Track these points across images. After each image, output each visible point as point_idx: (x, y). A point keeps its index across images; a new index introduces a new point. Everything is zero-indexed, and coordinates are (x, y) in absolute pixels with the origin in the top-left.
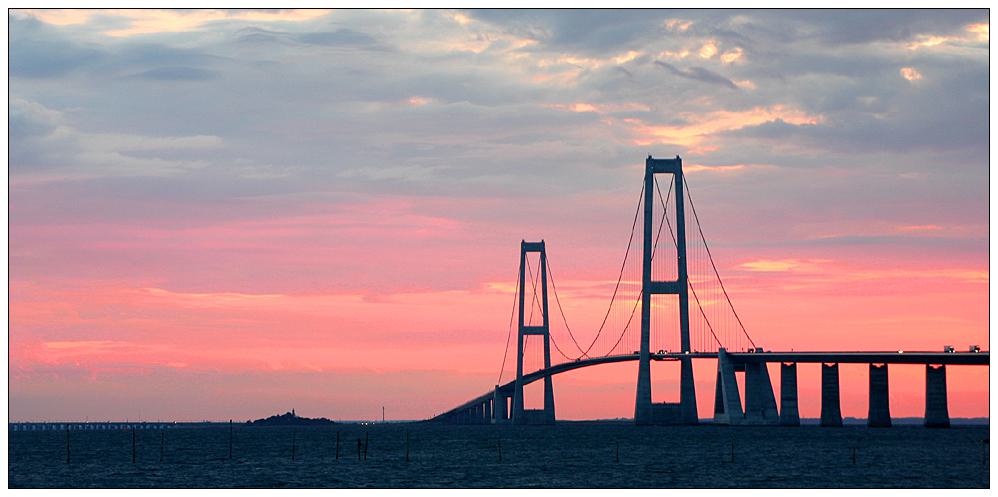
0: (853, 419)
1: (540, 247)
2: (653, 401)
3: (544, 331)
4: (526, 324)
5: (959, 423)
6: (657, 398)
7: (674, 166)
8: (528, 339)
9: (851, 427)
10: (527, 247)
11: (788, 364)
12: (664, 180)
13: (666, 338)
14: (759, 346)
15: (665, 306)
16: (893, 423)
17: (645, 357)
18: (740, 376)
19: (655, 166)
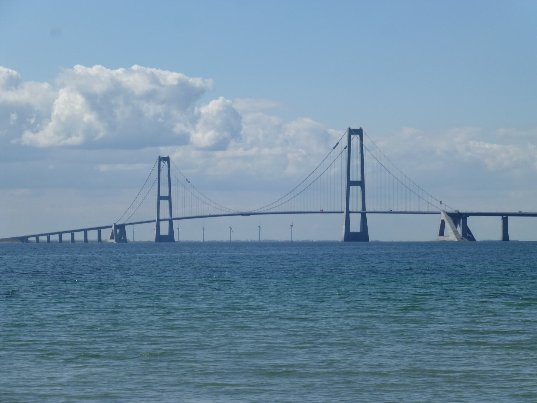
0: (515, 240)
1: (359, 132)
2: (160, 235)
3: (361, 183)
4: (351, 179)
5: (66, 241)
6: (352, 230)
7: (167, 159)
8: (161, 202)
9: (42, 242)
10: (351, 132)
11: (505, 217)
12: (164, 165)
13: (164, 214)
14: (391, 209)
15: (164, 204)
16: (39, 241)
17: (159, 220)
18: (118, 230)
19: (161, 159)
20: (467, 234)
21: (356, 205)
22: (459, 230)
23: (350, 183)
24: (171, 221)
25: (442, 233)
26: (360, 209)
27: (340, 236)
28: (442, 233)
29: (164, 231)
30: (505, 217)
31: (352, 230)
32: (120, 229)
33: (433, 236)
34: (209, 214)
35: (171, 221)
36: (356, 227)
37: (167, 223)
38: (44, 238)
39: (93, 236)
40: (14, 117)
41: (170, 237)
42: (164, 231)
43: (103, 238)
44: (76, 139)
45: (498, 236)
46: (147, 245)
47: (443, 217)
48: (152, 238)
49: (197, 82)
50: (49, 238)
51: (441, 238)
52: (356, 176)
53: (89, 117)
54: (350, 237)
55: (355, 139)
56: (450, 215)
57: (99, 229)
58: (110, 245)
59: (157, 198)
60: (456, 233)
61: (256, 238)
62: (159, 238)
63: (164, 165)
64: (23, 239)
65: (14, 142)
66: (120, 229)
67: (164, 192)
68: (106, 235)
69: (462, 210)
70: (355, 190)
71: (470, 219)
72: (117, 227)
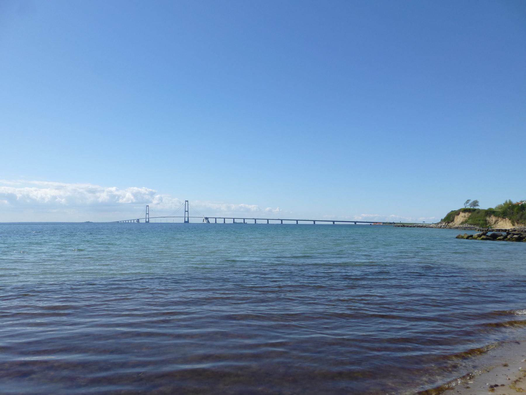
1: (188, 201)
6: (186, 221)
7: (148, 206)
10: (186, 201)
12: (148, 207)
15: (147, 215)
19: (147, 206)
20: (208, 221)
21: (187, 216)
22: (207, 221)
23: (185, 211)
24: (149, 218)
25: (203, 221)
26: (187, 216)
27: (183, 222)
28: (203, 221)
29: (147, 220)
30: (216, 218)
31: (186, 221)
32: (138, 220)
33: (202, 222)
34: (365, 221)
35: (149, 218)
36: (186, 220)
37: (148, 219)
38: (122, 222)
39: (132, 221)
40: (117, 197)
41: (188, 222)
42: (147, 220)
43: (135, 222)
44: (130, 202)
45: (223, 222)
46: (230, 224)
47: (204, 218)
48: (145, 222)
49: (154, 191)
50: (334, 223)
51: (203, 222)
52: (187, 210)
53: (132, 198)
54: (185, 222)
55: (187, 202)
56: (205, 218)
57: (134, 220)
58: (135, 223)
59: (356, 221)
60: (206, 221)
61: (154, 222)
62: (146, 222)
63: (148, 207)
64: (118, 222)
65: (117, 202)
66: (138, 220)
67: (147, 213)
68: (135, 221)
69: (208, 217)
70: (187, 213)
71: (209, 219)
72: (137, 219)
